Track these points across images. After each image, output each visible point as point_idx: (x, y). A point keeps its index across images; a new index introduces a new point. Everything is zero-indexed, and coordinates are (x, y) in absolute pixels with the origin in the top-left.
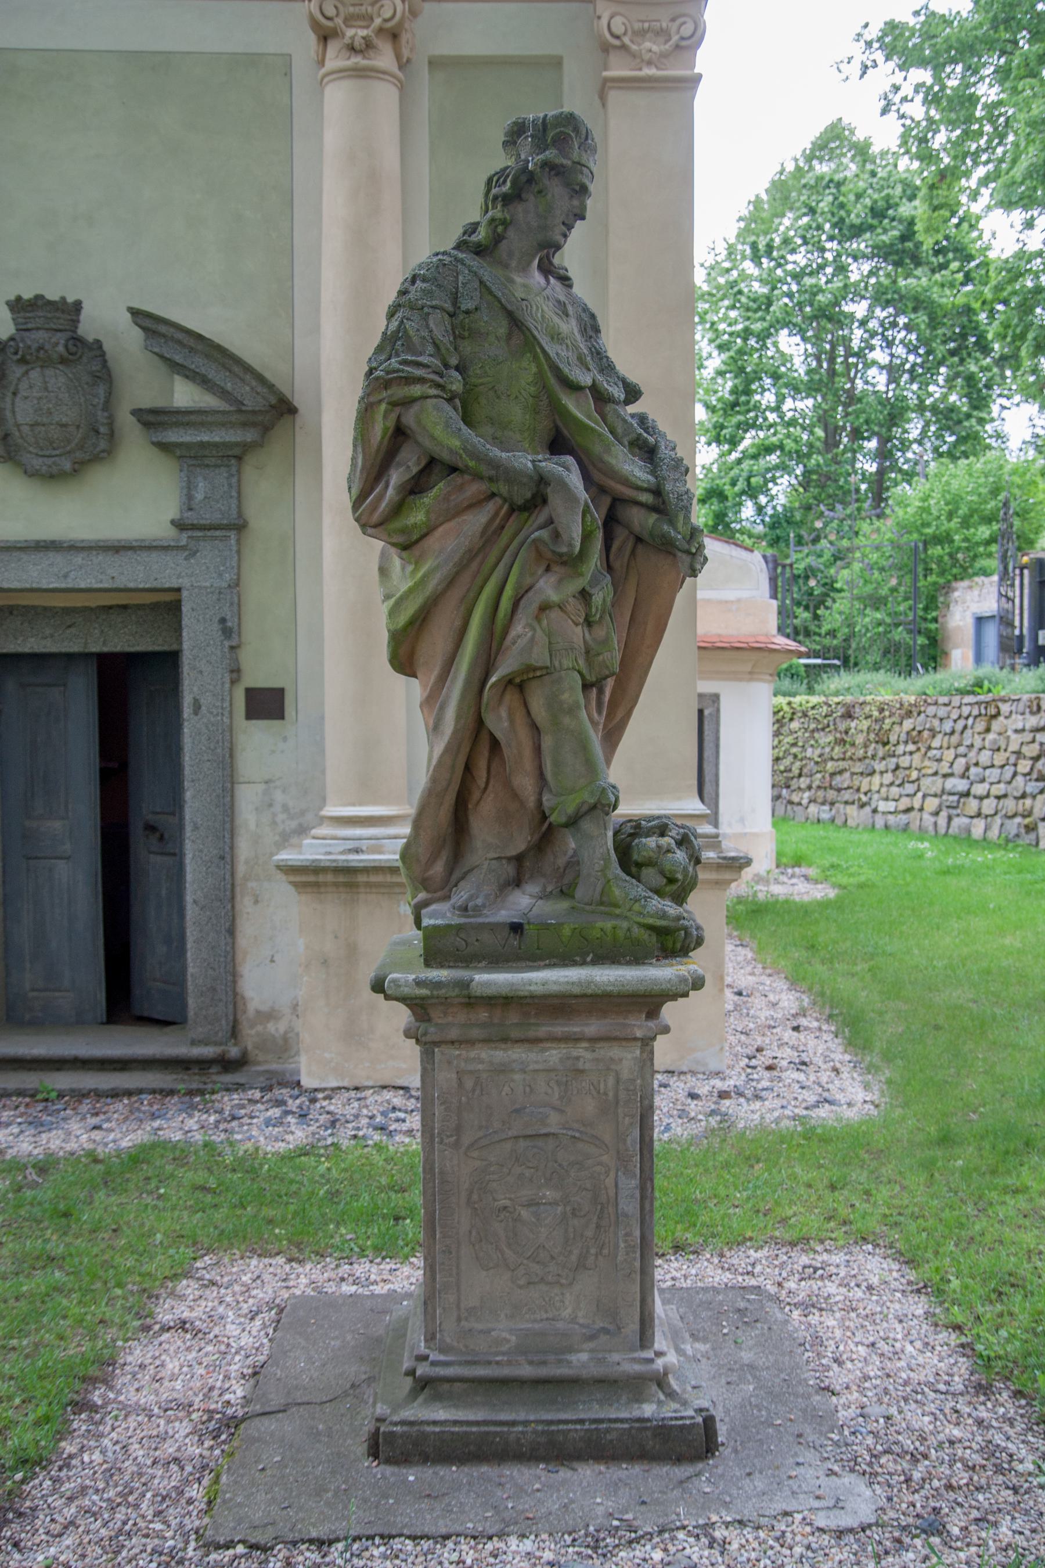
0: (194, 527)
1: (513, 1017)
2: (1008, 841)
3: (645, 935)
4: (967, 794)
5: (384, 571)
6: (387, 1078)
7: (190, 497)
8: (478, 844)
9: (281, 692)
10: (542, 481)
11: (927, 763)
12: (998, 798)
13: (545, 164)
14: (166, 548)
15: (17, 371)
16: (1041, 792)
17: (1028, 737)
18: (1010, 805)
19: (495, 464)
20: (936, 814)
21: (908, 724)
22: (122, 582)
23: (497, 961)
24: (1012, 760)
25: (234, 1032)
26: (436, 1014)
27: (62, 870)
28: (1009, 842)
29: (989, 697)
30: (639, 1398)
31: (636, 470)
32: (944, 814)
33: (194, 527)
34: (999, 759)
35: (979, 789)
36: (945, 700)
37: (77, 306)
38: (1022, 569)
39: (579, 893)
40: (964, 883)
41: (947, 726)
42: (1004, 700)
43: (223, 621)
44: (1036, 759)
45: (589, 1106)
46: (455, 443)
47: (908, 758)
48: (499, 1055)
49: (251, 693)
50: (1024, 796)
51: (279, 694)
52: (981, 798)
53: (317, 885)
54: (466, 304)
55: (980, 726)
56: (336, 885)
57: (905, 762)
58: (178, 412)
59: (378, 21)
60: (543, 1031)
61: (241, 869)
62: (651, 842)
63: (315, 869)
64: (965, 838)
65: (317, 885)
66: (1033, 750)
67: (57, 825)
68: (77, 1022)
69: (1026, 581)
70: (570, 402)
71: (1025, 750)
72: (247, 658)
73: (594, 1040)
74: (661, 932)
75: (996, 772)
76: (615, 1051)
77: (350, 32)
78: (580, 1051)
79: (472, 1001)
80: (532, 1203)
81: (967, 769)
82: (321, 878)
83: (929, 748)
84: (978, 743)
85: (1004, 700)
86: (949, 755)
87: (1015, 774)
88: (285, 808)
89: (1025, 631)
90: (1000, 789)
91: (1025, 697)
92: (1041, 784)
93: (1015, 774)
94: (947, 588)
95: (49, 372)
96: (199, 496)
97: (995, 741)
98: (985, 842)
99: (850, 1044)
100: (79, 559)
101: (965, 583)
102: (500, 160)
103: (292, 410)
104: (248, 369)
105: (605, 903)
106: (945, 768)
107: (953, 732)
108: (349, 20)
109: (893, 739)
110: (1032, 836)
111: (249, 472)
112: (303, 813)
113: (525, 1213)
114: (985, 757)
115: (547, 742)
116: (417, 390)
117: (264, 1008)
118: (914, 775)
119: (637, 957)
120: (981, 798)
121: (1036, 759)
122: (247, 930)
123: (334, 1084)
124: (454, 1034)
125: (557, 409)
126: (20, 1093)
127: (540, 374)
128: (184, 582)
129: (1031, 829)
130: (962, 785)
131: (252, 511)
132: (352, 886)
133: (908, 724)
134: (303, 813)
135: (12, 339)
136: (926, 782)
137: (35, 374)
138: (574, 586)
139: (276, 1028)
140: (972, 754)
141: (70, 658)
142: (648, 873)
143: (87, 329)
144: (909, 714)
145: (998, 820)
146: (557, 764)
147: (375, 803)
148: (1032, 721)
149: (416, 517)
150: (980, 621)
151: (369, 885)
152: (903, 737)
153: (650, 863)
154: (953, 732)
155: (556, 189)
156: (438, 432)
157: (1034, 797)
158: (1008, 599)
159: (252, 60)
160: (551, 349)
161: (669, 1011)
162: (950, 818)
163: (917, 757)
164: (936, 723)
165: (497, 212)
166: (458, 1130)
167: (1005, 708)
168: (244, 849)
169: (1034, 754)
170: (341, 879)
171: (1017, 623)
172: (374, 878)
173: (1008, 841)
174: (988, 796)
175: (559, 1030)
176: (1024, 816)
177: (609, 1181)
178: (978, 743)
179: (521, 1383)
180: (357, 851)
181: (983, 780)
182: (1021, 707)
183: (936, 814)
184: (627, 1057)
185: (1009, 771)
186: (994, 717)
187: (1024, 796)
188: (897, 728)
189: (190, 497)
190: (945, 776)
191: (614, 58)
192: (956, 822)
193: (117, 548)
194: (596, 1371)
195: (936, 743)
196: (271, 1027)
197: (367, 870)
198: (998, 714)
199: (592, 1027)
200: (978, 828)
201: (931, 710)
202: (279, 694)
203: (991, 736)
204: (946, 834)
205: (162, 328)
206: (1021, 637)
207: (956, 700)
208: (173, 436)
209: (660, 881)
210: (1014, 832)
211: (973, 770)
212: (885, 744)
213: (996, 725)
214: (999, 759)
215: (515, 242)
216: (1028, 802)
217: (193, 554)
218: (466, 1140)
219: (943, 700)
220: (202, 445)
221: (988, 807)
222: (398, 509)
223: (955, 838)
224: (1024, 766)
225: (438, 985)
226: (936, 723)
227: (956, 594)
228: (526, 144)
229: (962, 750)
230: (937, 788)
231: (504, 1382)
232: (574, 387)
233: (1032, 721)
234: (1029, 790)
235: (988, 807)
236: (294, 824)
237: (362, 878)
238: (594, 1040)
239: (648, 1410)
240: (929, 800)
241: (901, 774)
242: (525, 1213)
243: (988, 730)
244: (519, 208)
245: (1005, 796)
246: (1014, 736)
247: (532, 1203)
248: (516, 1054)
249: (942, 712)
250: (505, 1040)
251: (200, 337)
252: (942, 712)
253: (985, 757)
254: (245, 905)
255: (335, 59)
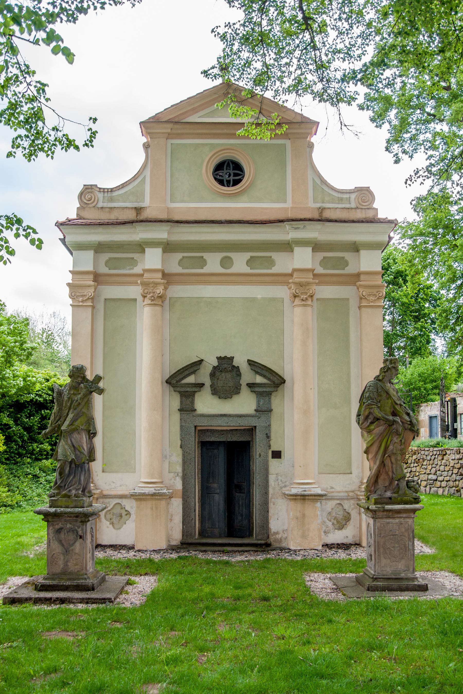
0: (260, 411)
1: (391, 514)
2: (451, 495)
3: (412, 499)
4: (436, 480)
5: (362, 436)
6: (312, 547)
7: (259, 404)
8: (380, 484)
9: (280, 452)
10: (394, 421)
11: (422, 470)
12: (447, 481)
13: (392, 367)
14: (253, 416)
15: (219, 374)
16: (461, 479)
17: (456, 461)
18: (451, 483)
19: (386, 419)
20: (426, 487)
21: (414, 457)
22: (242, 424)
23: (387, 504)
24: (451, 469)
25: (268, 537)
26: (377, 513)
27: (216, 496)
28: (451, 495)
29: (442, 448)
30: (414, 581)
31: (407, 418)
32: (428, 487)
33: (260, 411)
34: (447, 468)
35: (440, 478)
36: (428, 449)
37: (232, 359)
38: (447, 402)
39: (400, 492)
40: (439, 507)
41: (429, 458)
42: (448, 450)
43: (267, 434)
44: (459, 469)
45: (403, 530)
46: (380, 415)
47: (415, 468)
48: (388, 520)
49: (273, 452)
50: (455, 481)
51: (280, 452)
52: (441, 481)
53: (296, 499)
54: (379, 391)
55: (440, 458)
56: (300, 499)
57: (414, 469)
58: (259, 384)
59: (309, 294)
60: (396, 516)
61: (270, 496)
62: (412, 483)
63: (296, 495)
64: (436, 494)
65: (296, 499)
66: (458, 466)
67: (215, 485)
68: (220, 537)
69: (449, 405)
70: (396, 407)
71: (455, 465)
72: (272, 443)
73: (404, 518)
74: (415, 499)
75: (446, 473)
76: (408, 520)
77: (302, 296)
78: (402, 520)
79: (385, 511)
80: (394, 547)
81: (436, 472)
82: (297, 497)
83: (422, 465)
84: (439, 463)
85: (448, 450)
86: (430, 467)
87: (452, 474)
88: (281, 481)
89: (449, 424)
90: (448, 478)
91: (455, 449)
92: (461, 477)
93: (452, 474)
94: (418, 406)
95: (227, 374)
96: (261, 404)
97: (445, 463)
98: (443, 496)
99: (423, 542)
100: (231, 419)
101: (425, 404)
102: (382, 366)
103: (283, 381)
104: (277, 374)
105: (405, 495)
106: (428, 471)
107: (430, 460)
108: (302, 293)
109: (409, 462)
110: (459, 493)
111: (273, 397)
112: (286, 482)
113: (392, 549)
114: (442, 468)
115: (394, 466)
116: (373, 406)
117: (275, 531)
118: (417, 474)
119: (411, 503)
120: (441, 481)
121: (459, 469)
122: (271, 511)
123: (299, 548)
124: (380, 516)
125: (394, 408)
126: (219, 551)
127: (392, 402)
128: (257, 425)
129: (458, 491)
130: (434, 477)
131: (273, 407)
132: (304, 499)
133: (414, 457)
134: (286, 482)
135: (217, 366)
136: (421, 476)
137: (223, 374)
138: (399, 440)
139: (278, 536)
140: (438, 467)
141: (219, 443)
142: (412, 489)
143: (235, 363)
144: (415, 454)
145: (447, 489)
146: (396, 470)
147: (308, 479)
148: (458, 456)
149: (372, 427)
150: (431, 418)
151: (308, 499)
152: (413, 461)
153: (412, 487)
154: (430, 460)
155: (393, 370)
156: (377, 413)
157: (459, 481)
158: (443, 412)
159: (274, 300)
160: (394, 398)
161: (417, 513)
162: (430, 488)
163: (418, 468)
164: (425, 457)
165: (383, 374)
166: (380, 534)
167: (448, 452)
168: (271, 491)
169: (459, 467)
170: (302, 498)
171: (446, 420)
172: (310, 498)
173: (451, 495)
174: (443, 481)
175: (399, 516)
176: (456, 487)
177: (407, 543)
178: (439, 463)
179: (392, 579)
180: (305, 491)
181: (441, 476)
182: (454, 452)
183: (426, 487)
184: (410, 521)
185: (450, 473)
186: (445, 455)
187: (455, 481)
188: (410, 458)
189: (259, 404)
190: (428, 474)
191: (363, 301)
192: (433, 489)
193: (241, 416)
194: (405, 577)
195: (425, 463)
196: (277, 536)
197: (308, 495)
198: (446, 454)
199: (404, 515)
200: (440, 491)
201: (422, 452)
202: (280, 452)
203: (444, 461)
204: (429, 493)
205: (256, 364)
206: (448, 425)
207: (431, 449)
208: (257, 389)
209: (414, 490)
210: (453, 492)
211: (438, 472)
212: (406, 464)
213: (445, 458)
214: (447, 468)
215: (386, 379)
216: (457, 482)
217: (259, 418)
218: (382, 536)
219: (426, 449)
220: (263, 391)
221: (444, 484)
222: (368, 426)
223: (433, 494)
224: (455, 471)
225: (379, 507)
226: (425, 457)
227: (422, 408)
228: (388, 363)
229: (434, 466)
230: (425, 478)
231: (389, 579)
232: (396, 404)
233: (458, 456)
234: (457, 479)
235: (444, 484)
236: (283, 485)
237: (307, 497)
238: (404, 518)
239: (416, 583)
240: (423, 482)
241: (413, 473)
242: (392, 549)
243: (443, 459)
244: (387, 373)
245: (449, 481)
246: (451, 461)
247: (394, 547)
248: (391, 520)
249: (427, 453)
250: (389, 517)
251: (265, 367)
252: (427, 453)
253: (442, 468)
254: (271, 505)
255: (297, 302)
